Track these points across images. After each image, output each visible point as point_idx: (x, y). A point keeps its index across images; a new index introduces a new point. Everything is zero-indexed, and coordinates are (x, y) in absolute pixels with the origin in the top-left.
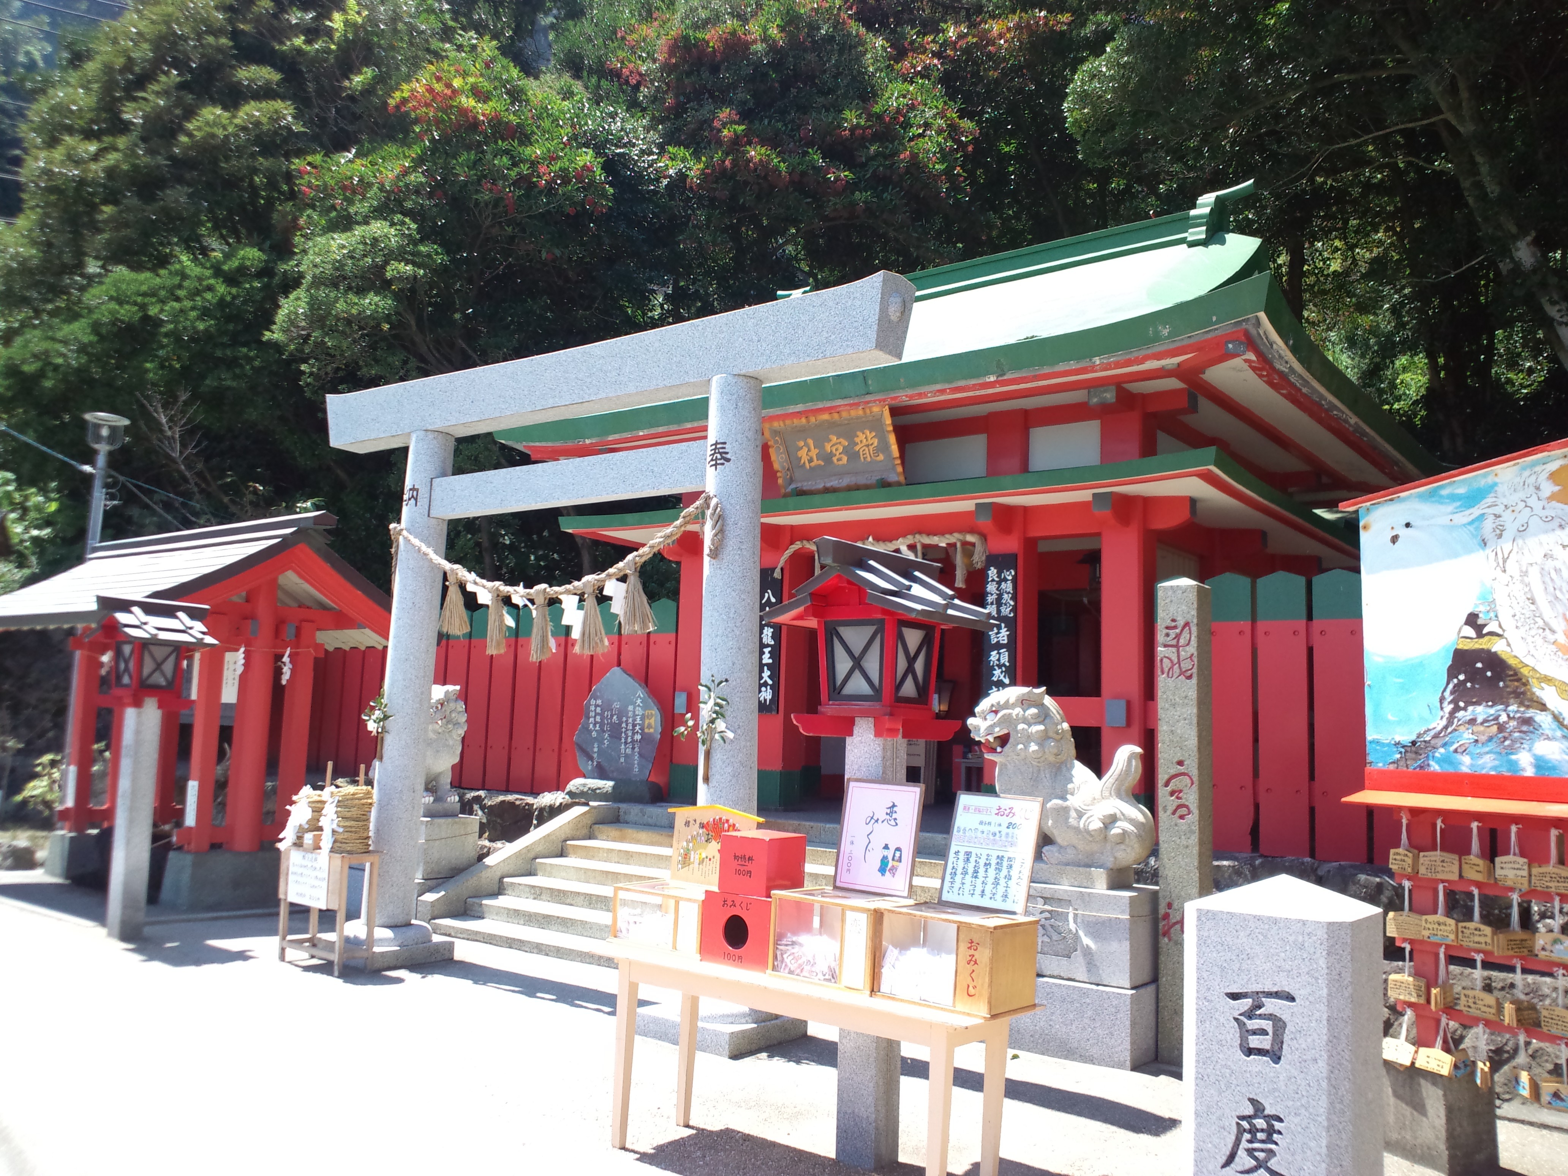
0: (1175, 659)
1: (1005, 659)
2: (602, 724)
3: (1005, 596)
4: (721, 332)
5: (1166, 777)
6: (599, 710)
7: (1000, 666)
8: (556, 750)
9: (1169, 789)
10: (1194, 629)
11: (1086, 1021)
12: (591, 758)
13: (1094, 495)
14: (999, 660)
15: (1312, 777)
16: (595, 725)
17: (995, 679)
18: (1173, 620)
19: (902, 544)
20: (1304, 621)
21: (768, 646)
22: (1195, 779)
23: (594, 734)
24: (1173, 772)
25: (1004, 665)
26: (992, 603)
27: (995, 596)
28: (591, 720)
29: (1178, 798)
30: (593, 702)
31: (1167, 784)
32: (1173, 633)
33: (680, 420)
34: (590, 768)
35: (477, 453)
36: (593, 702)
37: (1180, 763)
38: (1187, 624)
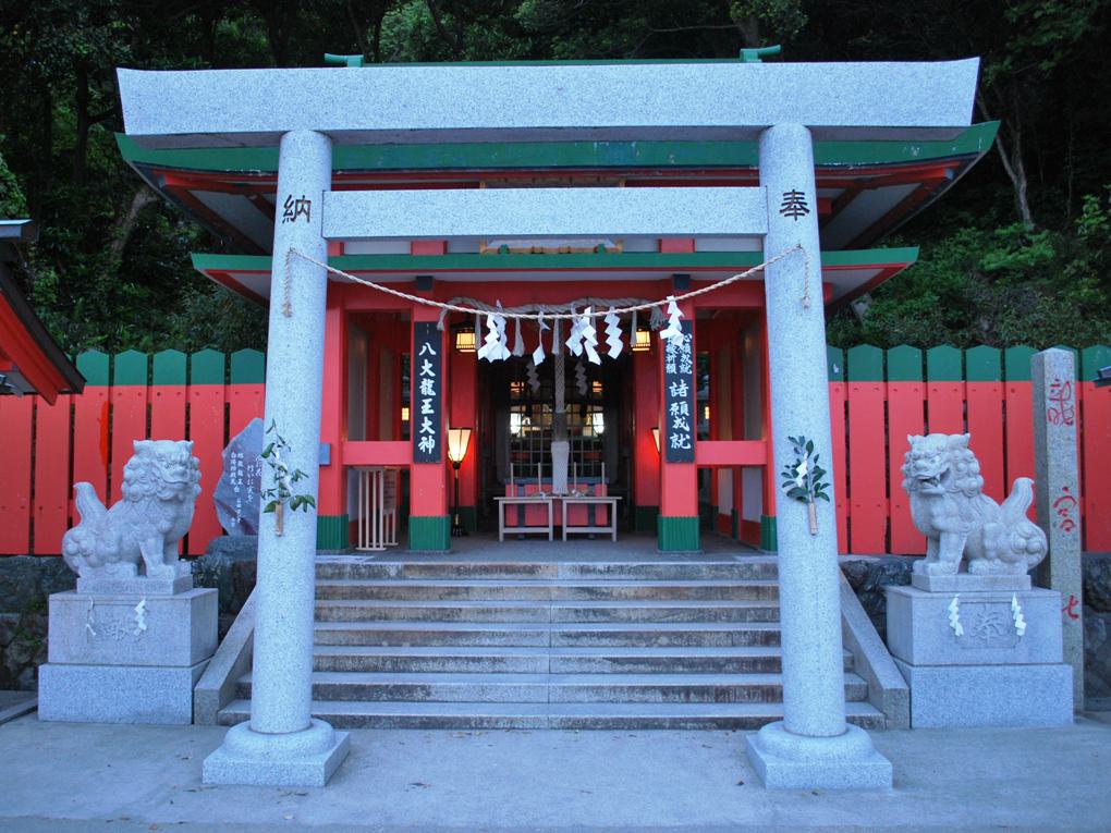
0: (1059, 409)
1: (685, 409)
2: (244, 479)
3: (684, 356)
4: (789, 81)
5: (1055, 500)
6: (240, 464)
7: (680, 416)
8: (27, 507)
9: (1057, 509)
10: (1073, 387)
11: (1039, 693)
12: (235, 515)
13: (418, 277)
14: (679, 411)
15: (888, 495)
16: (237, 480)
17: (676, 427)
18: (1057, 380)
19: (613, 311)
20: (184, 386)
21: (428, 397)
22: (1077, 501)
23: (237, 489)
24: (1060, 496)
25: (684, 415)
26: (671, 362)
27: (674, 356)
28: (233, 474)
29: (1065, 515)
30: (234, 455)
31: (1056, 505)
32: (1057, 390)
33: (729, 159)
34: (233, 524)
35: (362, 163)
36: (234, 455)
37: (1066, 489)
38: (1068, 383)
